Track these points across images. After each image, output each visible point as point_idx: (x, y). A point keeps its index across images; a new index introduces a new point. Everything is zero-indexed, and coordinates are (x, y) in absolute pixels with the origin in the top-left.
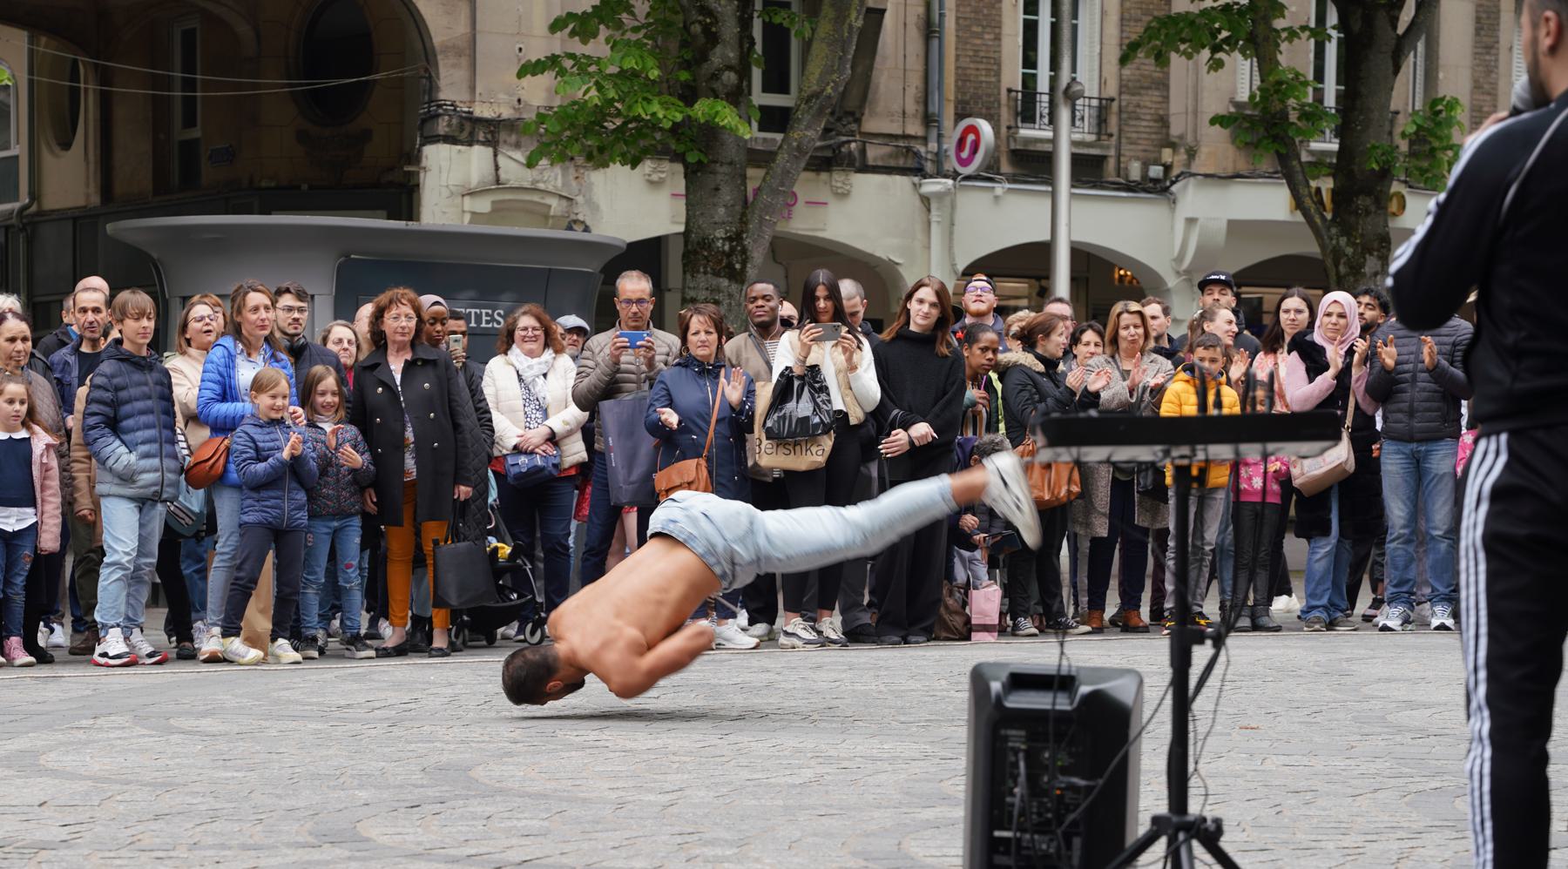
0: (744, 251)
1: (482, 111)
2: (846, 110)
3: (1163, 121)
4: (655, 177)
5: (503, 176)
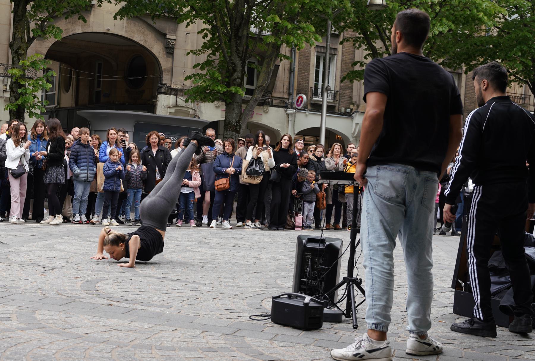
0: (240, 125)
1: (174, 86)
2: (269, 90)
3: (351, 98)
4: (217, 105)
5: (178, 103)
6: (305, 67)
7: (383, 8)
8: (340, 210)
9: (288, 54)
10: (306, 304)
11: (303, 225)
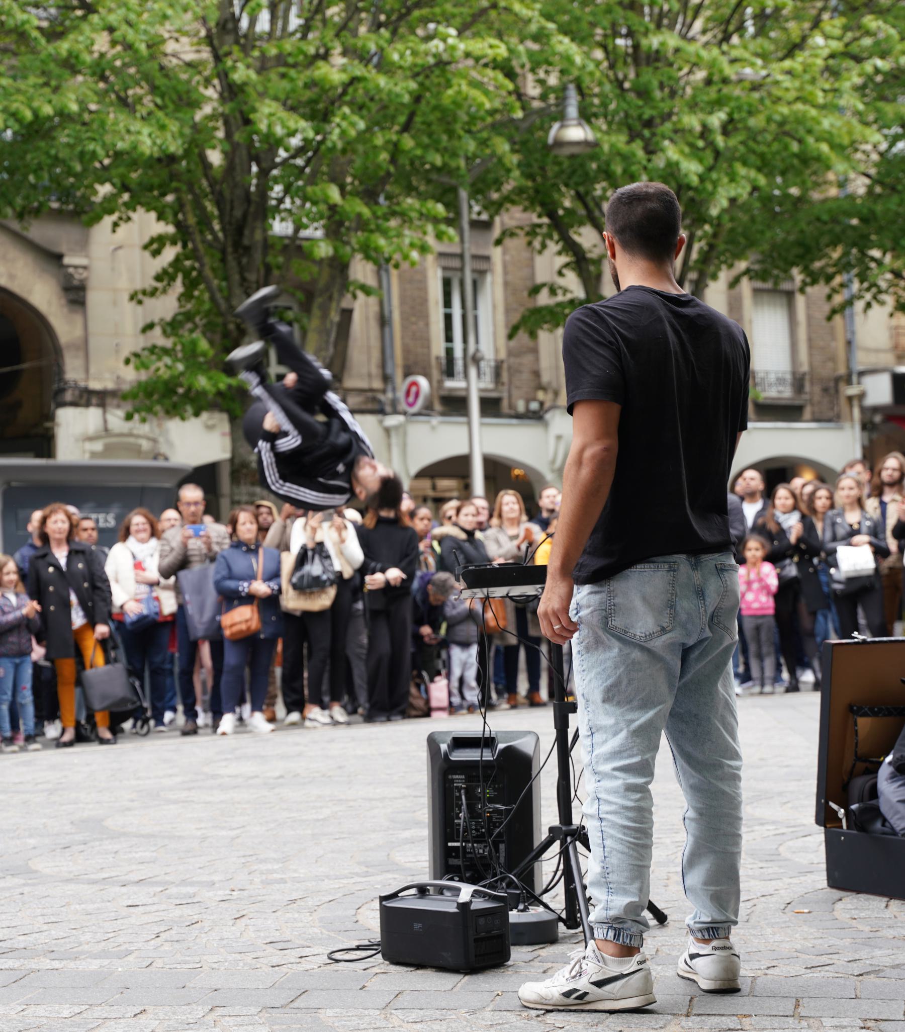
1: (95, 385)
3: (537, 374)
4: (210, 423)
6: (416, 308)
7: (588, 150)
8: (522, 662)
9: (371, 281)
10: (464, 907)
11: (450, 703)
